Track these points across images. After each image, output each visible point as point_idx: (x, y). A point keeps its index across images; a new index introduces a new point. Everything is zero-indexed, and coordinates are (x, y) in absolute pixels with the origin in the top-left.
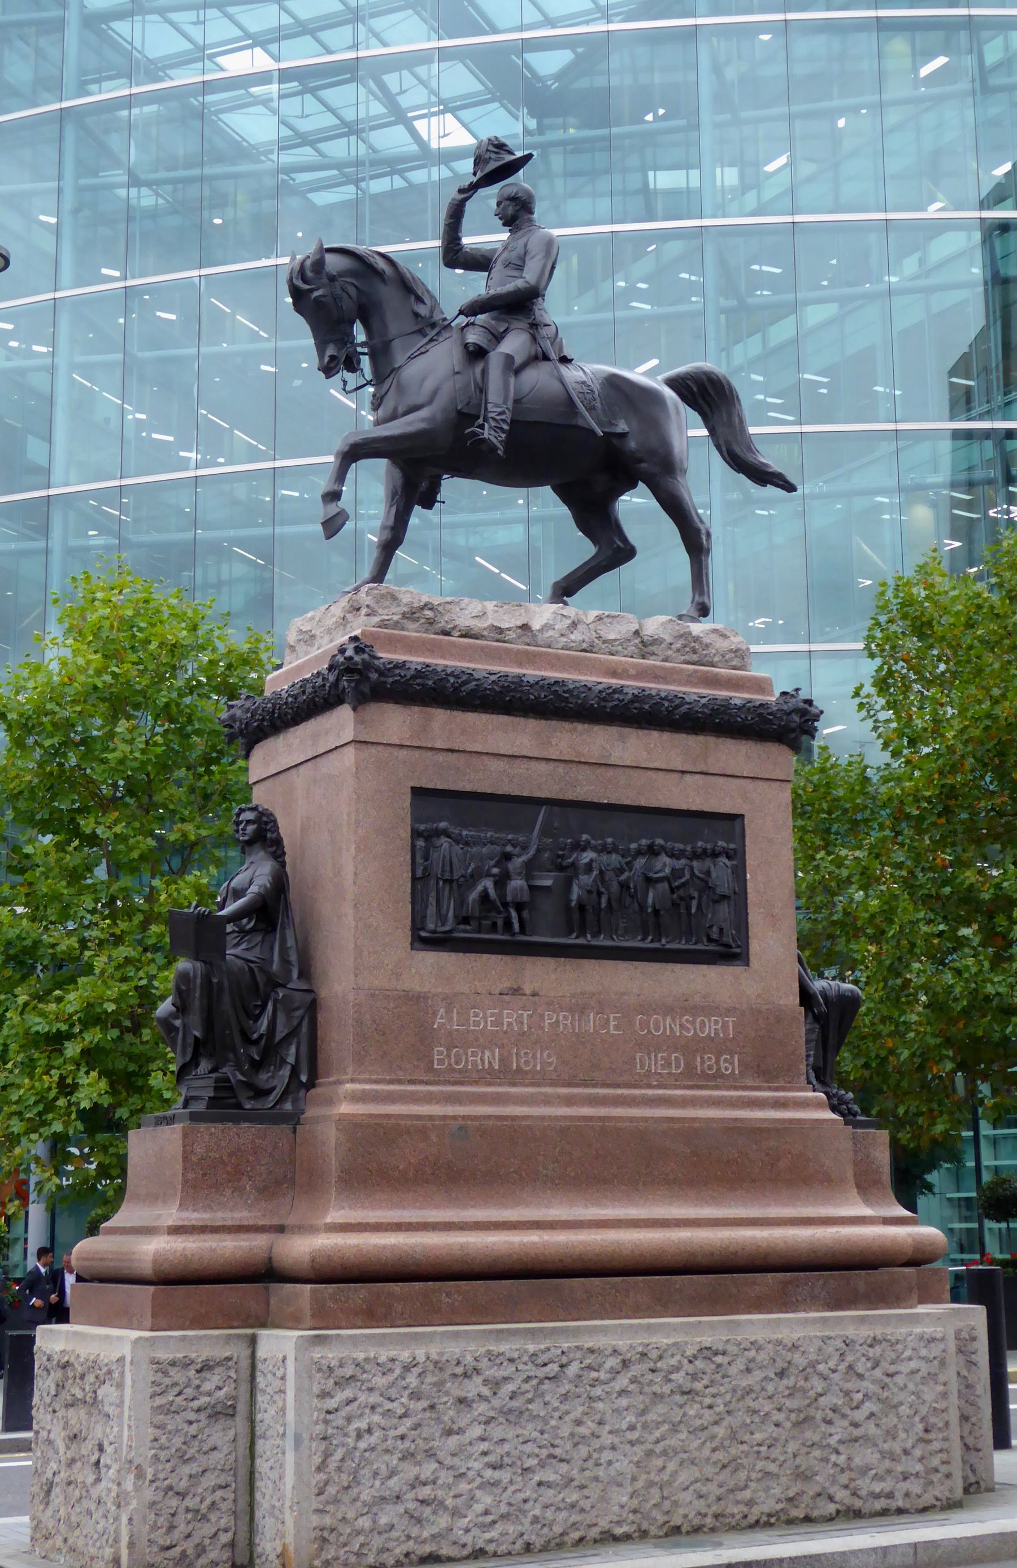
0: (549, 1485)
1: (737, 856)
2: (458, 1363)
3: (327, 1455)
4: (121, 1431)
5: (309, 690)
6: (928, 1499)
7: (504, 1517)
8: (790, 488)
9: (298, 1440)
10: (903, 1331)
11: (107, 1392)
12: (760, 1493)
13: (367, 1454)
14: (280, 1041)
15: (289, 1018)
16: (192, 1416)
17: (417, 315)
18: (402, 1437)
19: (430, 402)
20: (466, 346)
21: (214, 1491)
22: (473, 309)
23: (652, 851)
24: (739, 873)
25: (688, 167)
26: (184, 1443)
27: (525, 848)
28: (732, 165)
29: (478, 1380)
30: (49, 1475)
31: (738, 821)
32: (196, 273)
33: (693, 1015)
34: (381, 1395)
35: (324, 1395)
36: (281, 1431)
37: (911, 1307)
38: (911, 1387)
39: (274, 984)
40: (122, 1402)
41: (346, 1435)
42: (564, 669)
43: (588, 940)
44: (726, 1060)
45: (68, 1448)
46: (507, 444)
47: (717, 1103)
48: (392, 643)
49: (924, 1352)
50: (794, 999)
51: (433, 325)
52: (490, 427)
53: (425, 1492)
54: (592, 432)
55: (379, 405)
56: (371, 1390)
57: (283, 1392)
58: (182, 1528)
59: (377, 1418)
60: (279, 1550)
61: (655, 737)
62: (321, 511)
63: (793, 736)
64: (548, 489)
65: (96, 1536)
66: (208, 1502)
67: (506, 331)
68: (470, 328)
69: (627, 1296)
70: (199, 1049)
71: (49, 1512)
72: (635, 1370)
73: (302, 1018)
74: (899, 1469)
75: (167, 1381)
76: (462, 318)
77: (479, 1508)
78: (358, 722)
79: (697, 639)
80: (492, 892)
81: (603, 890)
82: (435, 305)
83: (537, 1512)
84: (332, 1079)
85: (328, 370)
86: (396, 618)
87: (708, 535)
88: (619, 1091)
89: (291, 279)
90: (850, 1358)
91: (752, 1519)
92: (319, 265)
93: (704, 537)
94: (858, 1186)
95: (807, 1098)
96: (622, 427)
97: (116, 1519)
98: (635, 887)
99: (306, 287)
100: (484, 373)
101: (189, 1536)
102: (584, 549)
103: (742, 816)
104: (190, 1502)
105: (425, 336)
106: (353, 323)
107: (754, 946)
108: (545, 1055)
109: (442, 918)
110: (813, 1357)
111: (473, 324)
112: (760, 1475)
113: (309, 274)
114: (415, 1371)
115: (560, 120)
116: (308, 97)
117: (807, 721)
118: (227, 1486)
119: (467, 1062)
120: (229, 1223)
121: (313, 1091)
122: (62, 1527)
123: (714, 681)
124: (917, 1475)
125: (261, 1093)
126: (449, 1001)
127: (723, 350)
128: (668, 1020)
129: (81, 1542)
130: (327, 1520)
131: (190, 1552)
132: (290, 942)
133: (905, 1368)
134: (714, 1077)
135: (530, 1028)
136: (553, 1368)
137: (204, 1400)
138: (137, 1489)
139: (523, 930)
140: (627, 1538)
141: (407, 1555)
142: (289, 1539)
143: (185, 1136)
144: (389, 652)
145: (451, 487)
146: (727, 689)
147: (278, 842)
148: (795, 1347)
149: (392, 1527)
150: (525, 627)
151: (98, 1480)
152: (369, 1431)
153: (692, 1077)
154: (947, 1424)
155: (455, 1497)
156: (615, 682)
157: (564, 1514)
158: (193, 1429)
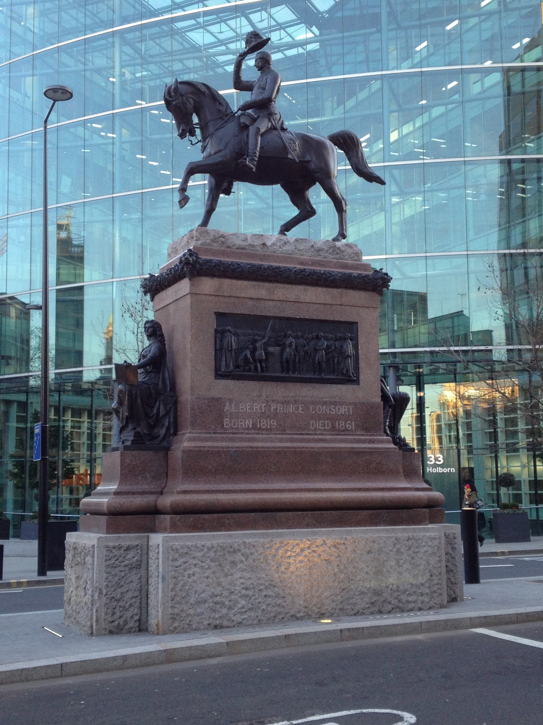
0: (269, 596)
1: (355, 340)
2: (231, 547)
3: (176, 584)
4: (93, 575)
5: (173, 272)
6: (432, 603)
7: (250, 609)
8: (382, 183)
9: (163, 578)
10: (422, 534)
11: (89, 559)
12: (359, 601)
13: (192, 584)
14: (162, 417)
15: (165, 407)
16: (122, 569)
17: (219, 111)
18: (208, 577)
20: (240, 124)
21: (131, 599)
22: (244, 108)
23: (318, 338)
24: (356, 347)
26: (119, 580)
27: (263, 337)
29: (239, 554)
30: (70, 592)
31: (355, 325)
33: (335, 405)
34: (199, 560)
35: (175, 560)
36: (157, 574)
37: (426, 525)
38: (425, 558)
40: (93, 563)
41: (183, 576)
42: (280, 262)
43: (291, 375)
44: (349, 424)
45: (76, 582)
46: (257, 167)
47: (345, 441)
48: (206, 251)
49: (430, 543)
50: (378, 400)
51: (227, 115)
53: (218, 599)
54: (294, 160)
56: (194, 558)
57: (158, 559)
58: (118, 614)
59: (197, 569)
60: (156, 623)
61: (320, 290)
62: (177, 197)
63: (379, 288)
64: (279, 186)
65: (85, 617)
66: (129, 603)
67: (258, 117)
68: (243, 116)
69: (304, 520)
70: (128, 420)
71: (70, 607)
73: (171, 407)
74: (419, 591)
75: (112, 555)
76: (240, 112)
77: (239, 606)
78: (192, 285)
79: (339, 248)
80: (249, 355)
81: (296, 354)
82: (227, 106)
83: (264, 607)
84: (182, 432)
85: (182, 135)
86: (208, 241)
88: (303, 437)
89: (165, 96)
90: (398, 546)
91: (355, 611)
92: (176, 89)
94: (405, 476)
95: (383, 439)
96: (308, 158)
97: (92, 610)
98: (311, 353)
99: (171, 99)
100: (248, 136)
101: (121, 617)
102: (295, 212)
103: (357, 323)
104: (121, 603)
105: (223, 120)
106: (192, 115)
107: (362, 377)
108: (271, 422)
109: (227, 366)
110: (382, 545)
112: (359, 593)
113: (173, 94)
114: (213, 550)
116: (223, 24)
117: (385, 282)
118: (137, 597)
119: (238, 425)
120: (140, 490)
121: (175, 437)
122: (74, 614)
123: (346, 266)
124: (427, 594)
125: (153, 438)
126: (230, 401)
128: (324, 407)
129: (80, 619)
130: (176, 611)
131: (121, 624)
132: (167, 375)
133: (422, 550)
134: (344, 431)
135: (265, 411)
137: (127, 562)
138: (99, 598)
139: (262, 370)
140: (301, 618)
141: (209, 624)
142: (160, 618)
143: (122, 455)
144: (205, 256)
146: (351, 269)
147: (162, 335)
148: (374, 542)
149: (203, 613)
150: (264, 244)
151: (86, 595)
152: (194, 575)
153: (282, 429)
154: (440, 574)
155: (229, 601)
156: (302, 267)
157: (276, 608)
158: (122, 574)
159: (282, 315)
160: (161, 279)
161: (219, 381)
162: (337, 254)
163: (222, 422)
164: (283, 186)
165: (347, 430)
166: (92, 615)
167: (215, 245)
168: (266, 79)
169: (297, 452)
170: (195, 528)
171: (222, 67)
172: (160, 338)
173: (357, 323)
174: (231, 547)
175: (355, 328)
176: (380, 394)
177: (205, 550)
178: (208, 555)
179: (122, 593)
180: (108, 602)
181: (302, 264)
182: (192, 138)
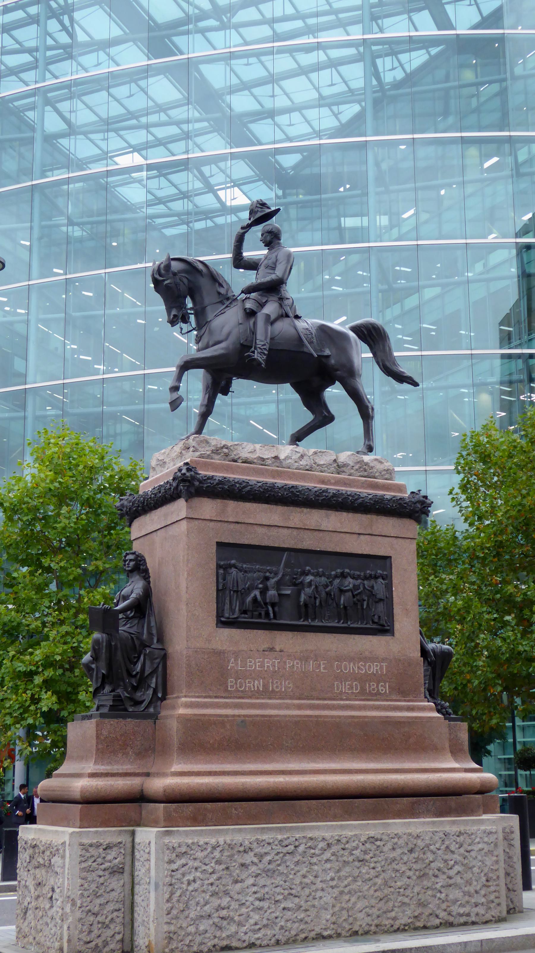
0: (289, 909)
1: (388, 578)
2: (241, 845)
3: (172, 894)
4: (64, 881)
5: (162, 491)
6: (488, 917)
7: (265, 926)
8: (416, 384)
10: (475, 828)
12: (400, 914)
13: (193, 893)
15: (152, 663)
16: (101, 873)
17: (219, 293)
18: (212, 884)
19: (226, 339)
20: (245, 309)
23: (343, 576)
24: (389, 587)
25: (362, 215)
26: (97, 887)
27: (276, 574)
28: (385, 214)
29: (251, 854)
31: (388, 560)
32: (103, 271)
33: (365, 662)
34: (201, 862)
35: (171, 862)
36: (148, 881)
38: (479, 858)
39: (144, 646)
40: (64, 866)
41: (182, 883)
42: (297, 480)
43: (309, 622)
44: (382, 686)
45: (36, 890)
47: (378, 708)
48: (206, 466)
49: (486, 839)
50: (417, 654)
51: (228, 299)
52: (258, 353)
53: (224, 913)
54: (312, 355)
55: (200, 341)
56: (195, 859)
57: (149, 860)
58: (96, 932)
59: (198, 874)
60: (147, 944)
62: (169, 397)
63: (417, 515)
65: (50, 936)
66: (109, 918)
67: (266, 302)
69: (330, 810)
70: (105, 680)
71: (26, 924)
72: (334, 849)
73: (159, 664)
75: (88, 855)
76: (243, 295)
77: (252, 921)
78: (189, 507)
79: (367, 464)
80: (259, 597)
81: (317, 596)
82: (229, 288)
83: (283, 923)
84: (174, 696)
85: (173, 322)
86: (208, 453)
87: (373, 409)
88: (326, 702)
90: (447, 843)
91: (396, 927)
92: (168, 267)
93: (370, 410)
95: (425, 706)
96: (327, 352)
97: (61, 927)
100: (255, 324)
101: (99, 936)
102: (307, 417)
103: (390, 557)
104: (100, 918)
107: (397, 626)
108: (287, 683)
109: (232, 611)
110: (428, 842)
111: (249, 298)
112: (400, 904)
113: (163, 272)
114: (219, 849)
115: (295, 191)
117: (424, 507)
118: (119, 910)
119: (246, 686)
120: (121, 771)
121: (164, 702)
122: (33, 932)
124: (482, 904)
125: (138, 703)
126: (236, 655)
127: (380, 312)
129: (42, 940)
130: (172, 928)
132: (153, 624)
133: (476, 848)
134: (376, 694)
135: (279, 669)
136: (291, 848)
137: (107, 865)
138: (72, 911)
139: (275, 617)
140: (330, 937)
141: (214, 946)
142: (152, 938)
143: (97, 725)
144: (205, 471)
145: (238, 384)
147: (146, 571)
150: (276, 458)
151: (52, 907)
155: (240, 915)
156: (324, 487)
157: (297, 925)
158: (101, 880)
159: (299, 546)
160: (144, 499)
161: (222, 630)
162: (365, 471)
163: (226, 684)
164: (292, 385)
165: (380, 694)
166: (62, 934)
167: (217, 457)
168: (276, 257)
169: (318, 722)
170: (195, 820)
171: (159, 230)
172: (144, 574)
173: (390, 557)
174: (241, 845)
175: (388, 564)
176: (419, 647)
177: (209, 850)
178: (212, 856)
179: (100, 905)
180: (83, 916)
181: (323, 482)
182: (184, 326)
